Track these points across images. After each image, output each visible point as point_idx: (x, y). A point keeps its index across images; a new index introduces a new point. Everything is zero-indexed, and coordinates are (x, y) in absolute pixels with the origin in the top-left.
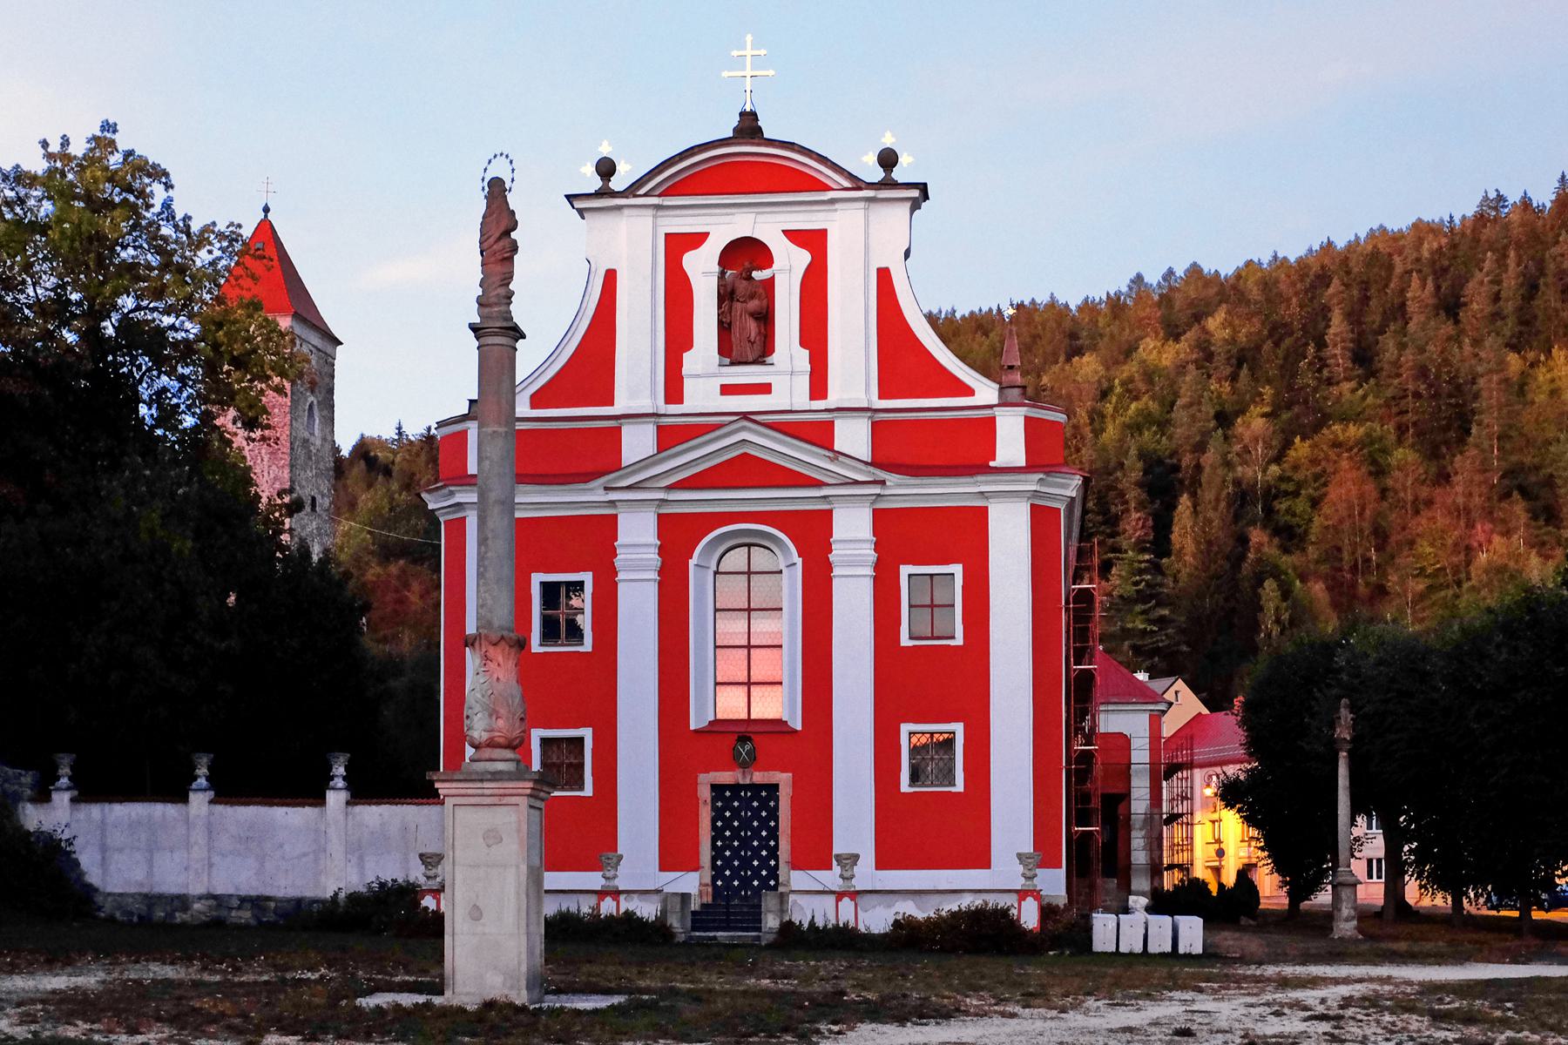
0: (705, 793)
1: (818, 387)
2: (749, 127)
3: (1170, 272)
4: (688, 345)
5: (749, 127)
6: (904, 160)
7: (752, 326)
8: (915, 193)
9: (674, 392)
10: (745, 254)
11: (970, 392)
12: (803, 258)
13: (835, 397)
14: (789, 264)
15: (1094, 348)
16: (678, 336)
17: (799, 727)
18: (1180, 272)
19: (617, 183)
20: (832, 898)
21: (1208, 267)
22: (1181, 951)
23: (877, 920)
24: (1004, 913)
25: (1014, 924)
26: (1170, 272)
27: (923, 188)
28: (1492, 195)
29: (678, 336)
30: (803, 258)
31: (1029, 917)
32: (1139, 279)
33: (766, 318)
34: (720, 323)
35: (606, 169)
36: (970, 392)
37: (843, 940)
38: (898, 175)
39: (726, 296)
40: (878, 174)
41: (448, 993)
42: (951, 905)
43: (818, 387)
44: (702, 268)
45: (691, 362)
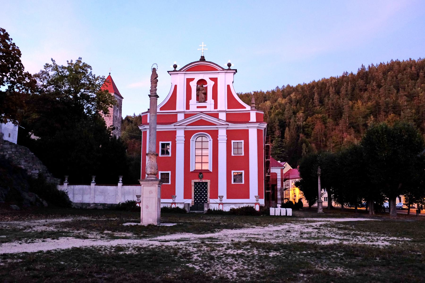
0: (193, 184)
1: (216, 107)
2: (203, 59)
3: (284, 86)
4: (191, 99)
5: (203, 59)
6: (232, 65)
7: (203, 95)
8: (235, 71)
9: (188, 107)
10: (202, 82)
11: (245, 108)
12: (213, 83)
13: (218, 109)
14: (210, 84)
15: (269, 100)
16: (189, 97)
17: (211, 171)
18: (286, 86)
19: (177, 69)
20: (218, 204)
21: (291, 85)
22: (288, 215)
23: (227, 209)
24: (252, 207)
25: (254, 210)
26: (284, 86)
27: (236, 70)
28: (345, 72)
29: (189, 97)
30: (213, 83)
31: (257, 208)
32: (278, 87)
33: (206, 94)
34: (197, 95)
35: (175, 66)
36: (245, 108)
37: (220, 213)
38: (231, 68)
39: (198, 90)
40: (227, 68)
41: (141, 223)
42: (242, 206)
43: (216, 107)
44: (194, 85)
45: (191, 102)
